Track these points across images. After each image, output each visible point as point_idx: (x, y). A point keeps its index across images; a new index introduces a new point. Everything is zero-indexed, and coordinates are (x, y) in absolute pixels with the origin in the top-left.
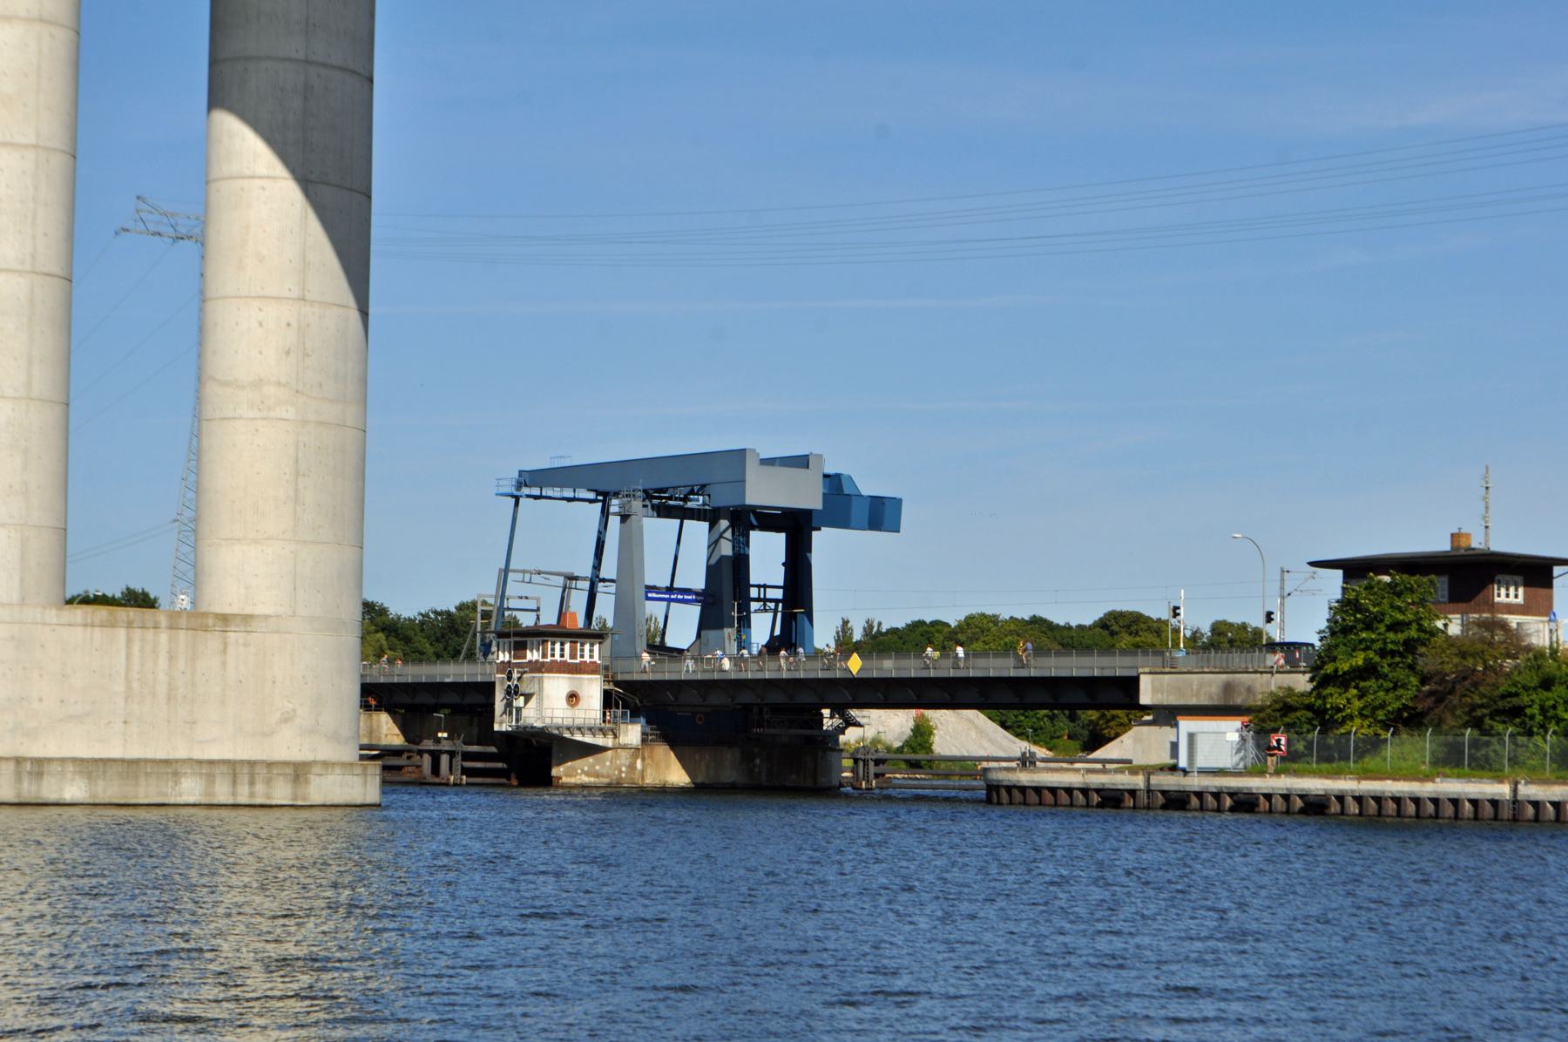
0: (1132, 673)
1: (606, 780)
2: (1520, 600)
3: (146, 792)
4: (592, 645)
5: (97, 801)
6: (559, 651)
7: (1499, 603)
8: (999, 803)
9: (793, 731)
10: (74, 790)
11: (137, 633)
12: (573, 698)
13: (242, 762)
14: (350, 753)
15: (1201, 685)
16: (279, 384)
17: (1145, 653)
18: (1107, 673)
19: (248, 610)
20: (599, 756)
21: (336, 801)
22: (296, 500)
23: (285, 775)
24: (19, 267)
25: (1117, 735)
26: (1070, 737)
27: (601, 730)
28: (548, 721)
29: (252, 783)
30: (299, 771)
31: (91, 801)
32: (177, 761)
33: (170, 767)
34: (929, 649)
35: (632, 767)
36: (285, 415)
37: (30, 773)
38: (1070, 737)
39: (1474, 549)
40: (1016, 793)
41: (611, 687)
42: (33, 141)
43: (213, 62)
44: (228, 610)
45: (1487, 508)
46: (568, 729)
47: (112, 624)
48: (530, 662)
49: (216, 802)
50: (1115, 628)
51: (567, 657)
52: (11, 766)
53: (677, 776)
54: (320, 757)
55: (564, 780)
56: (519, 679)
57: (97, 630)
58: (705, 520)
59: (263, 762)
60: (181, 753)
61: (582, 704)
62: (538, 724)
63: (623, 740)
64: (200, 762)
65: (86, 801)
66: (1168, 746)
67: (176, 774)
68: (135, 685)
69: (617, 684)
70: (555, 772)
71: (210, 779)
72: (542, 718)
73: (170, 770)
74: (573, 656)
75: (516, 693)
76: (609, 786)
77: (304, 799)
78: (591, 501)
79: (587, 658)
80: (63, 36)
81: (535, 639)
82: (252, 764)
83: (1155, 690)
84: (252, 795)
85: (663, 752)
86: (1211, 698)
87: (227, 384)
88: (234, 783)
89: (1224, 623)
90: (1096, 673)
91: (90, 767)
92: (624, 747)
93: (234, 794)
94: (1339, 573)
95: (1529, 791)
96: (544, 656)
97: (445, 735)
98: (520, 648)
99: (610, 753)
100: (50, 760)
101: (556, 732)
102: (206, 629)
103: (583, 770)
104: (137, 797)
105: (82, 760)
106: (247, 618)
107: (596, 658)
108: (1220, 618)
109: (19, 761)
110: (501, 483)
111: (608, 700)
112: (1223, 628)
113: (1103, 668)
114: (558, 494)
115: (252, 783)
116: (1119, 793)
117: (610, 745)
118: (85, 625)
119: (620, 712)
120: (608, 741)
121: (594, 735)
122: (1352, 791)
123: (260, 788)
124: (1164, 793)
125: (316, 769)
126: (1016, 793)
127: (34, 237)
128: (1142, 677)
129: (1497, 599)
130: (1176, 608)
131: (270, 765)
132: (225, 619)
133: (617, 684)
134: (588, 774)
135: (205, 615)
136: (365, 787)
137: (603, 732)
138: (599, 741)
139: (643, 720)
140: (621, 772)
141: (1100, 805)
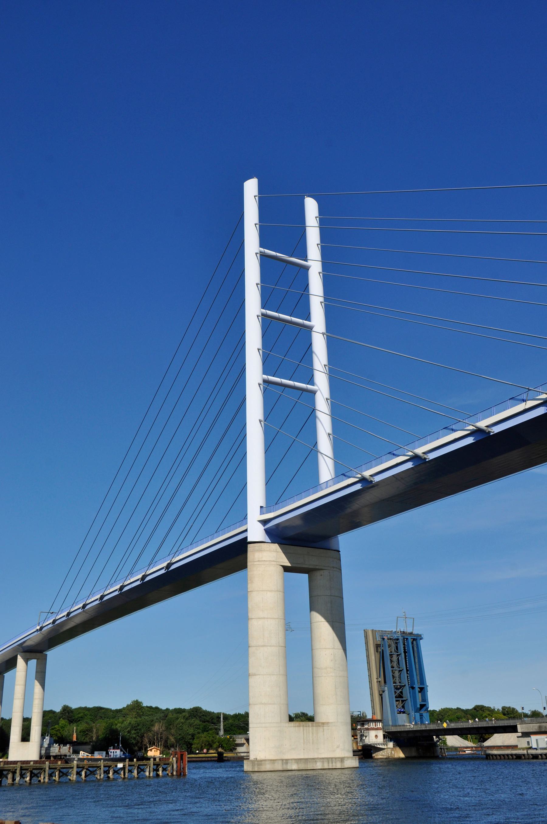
0: (515, 724)
1: (385, 757)
3: (310, 767)
4: (379, 723)
5: (300, 769)
6: (372, 725)
8: (490, 759)
9: (428, 742)
10: (295, 767)
11: (305, 728)
12: (376, 736)
13: (330, 758)
14: (351, 754)
15: (533, 726)
16: (330, 668)
17: (517, 719)
18: (509, 725)
19: (327, 721)
20: (383, 751)
21: (350, 767)
22: (336, 694)
23: (339, 761)
24: (276, 645)
25: (489, 738)
26: (475, 739)
27: (383, 744)
28: (371, 743)
29: (332, 763)
30: (342, 760)
31: (298, 769)
32: (316, 758)
33: (314, 760)
34: (470, 721)
35: (391, 753)
36: (332, 675)
37: (285, 763)
38: (475, 739)
40: (494, 756)
41: (384, 733)
42: (277, 617)
43: (311, 597)
44: (323, 721)
46: (376, 744)
47: (299, 726)
48: (366, 728)
49: (324, 768)
50: (478, 709)
51: (374, 726)
52: (281, 761)
53: (402, 755)
54: (346, 756)
55: (376, 757)
56: (363, 732)
57: (296, 728)
59: (334, 758)
60: (316, 757)
61: (378, 738)
62: (369, 743)
63: (389, 746)
64: (321, 758)
65: (297, 769)
66: (527, 742)
67: (316, 762)
68: (305, 740)
70: (373, 755)
71: (323, 762)
72: (369, 742)
73: (314, 761)
74: (375, 726)
75: (363, 736)
76: (386, 758)
77: (343, 766)
79: (379, 726)
80: (282, 594)
82: (332, 758)
83: (521, 729)
84: (332, 766)
85: (398, 749)
86: (536, 730)
87: (319, 669)
88: (328, 763)
89: (505, 707)
90: (506, 725)
91: (298, 761)
92: (389, 748)
93: (328, 766)
96: (369, 726)
98: (363, 725)
99: (386, 750)
100: (289, 759)
101: (373, 745)
102: (319, 726)
104: (308, 768)
105: (296, 759)
106: (328, 723)
107: (381, 726)
108: (504, 706)
109: (282, 760)
111: (384, 737)
112: (505, 708)
113: (507, 723)
115: (332, 763)
116: (520, 755)
117: (386, 748)
118: (294, 727)
119: (387, 739)
120: (385, 747)
121: (382, 745)
123: (334, 764)
124: (532, 755)
125: (346, 759)
126: (494, 756)
127: (279, 638)
128: (518, 725)
130: (523, 708)
131: (336, 758)
132: (323, 723)
133: (386, 732)
134: (381, 755)
135: (319, 723)
137: (384, 744)
138: (383, 747)
139: (393, 742)
140: (389, 754)
141: (516, 759)
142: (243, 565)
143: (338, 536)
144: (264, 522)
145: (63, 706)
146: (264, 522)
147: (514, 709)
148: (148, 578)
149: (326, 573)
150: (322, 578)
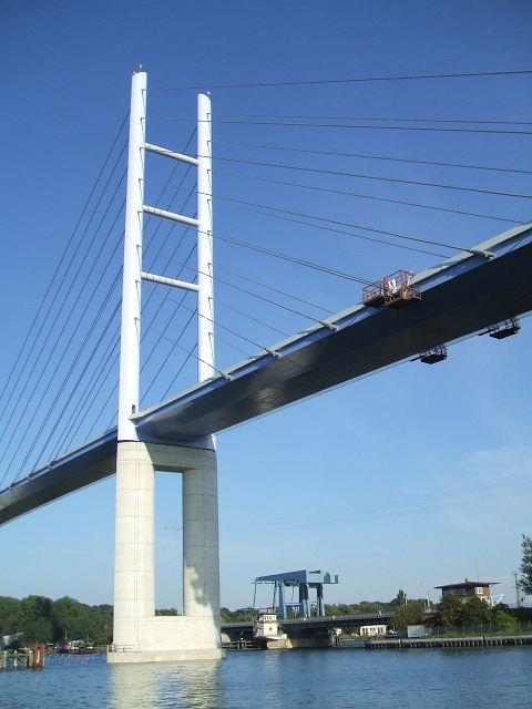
43: (184, 495)
95: (487, 638)
136: (219, 654)
143: (446, 344)
144: (136, 421)
146: (136, 421)
149: (199, 472)
150: (195, 476)
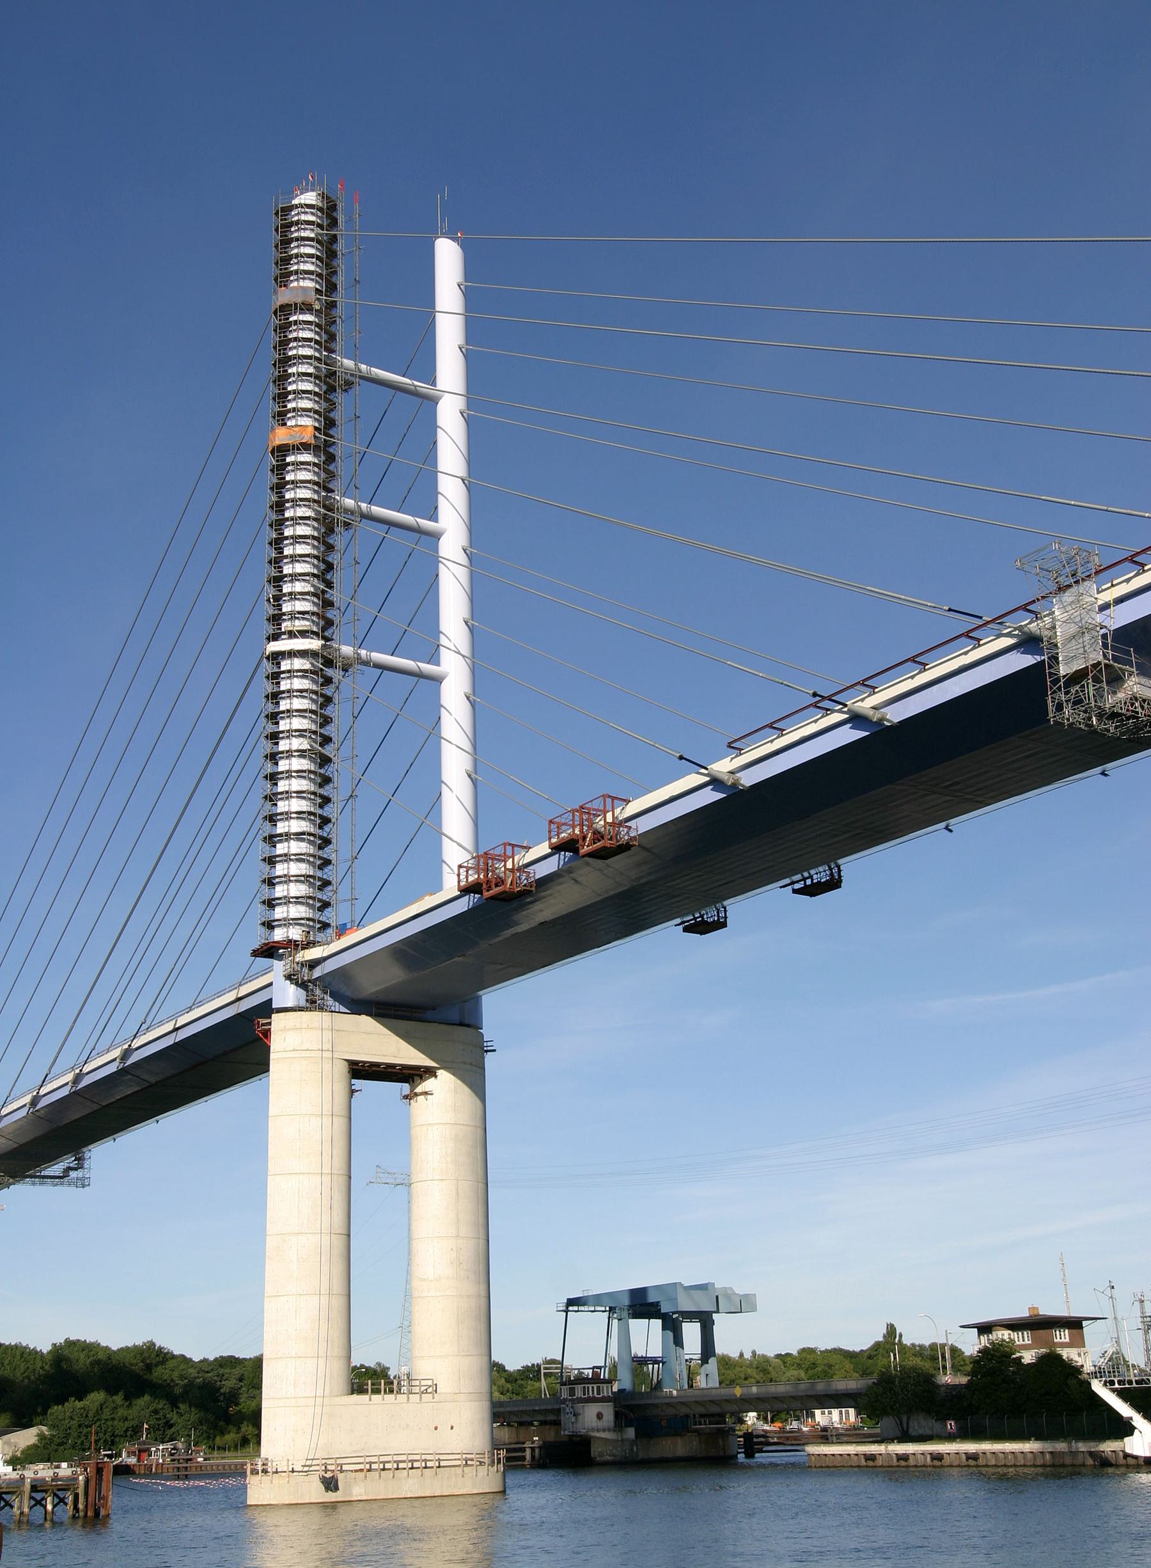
2: (1067, 1340)
7: (1056, 1343)
12: (600, 1416)
39: (1041, 1315)
45: (1064, 1275)
58: (659, 1319)
69: (622, 1406)
78: (603, 1311)
79: (606, 1394)
81: (579, 1386)
92: (628, 1440)
94: (976, 1329)
96: (584, 1395)
97: (537, 1438)
103: (607, 1453)
110: (558, 1305)
114: (587, 1309)
122: (990, 1450)
129: (1055, 1340)
136: (485, 1479)
140: (626, 1453)
142: (260, 1066)
143: (480, 993)
145: (500, 1363)
147: (933, 1343)
148: (43, 1103)
